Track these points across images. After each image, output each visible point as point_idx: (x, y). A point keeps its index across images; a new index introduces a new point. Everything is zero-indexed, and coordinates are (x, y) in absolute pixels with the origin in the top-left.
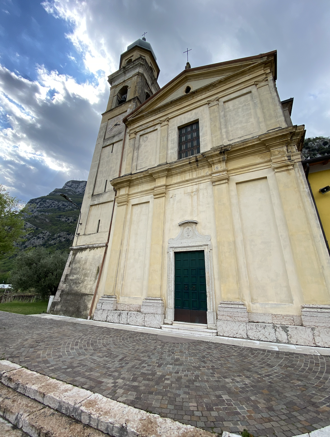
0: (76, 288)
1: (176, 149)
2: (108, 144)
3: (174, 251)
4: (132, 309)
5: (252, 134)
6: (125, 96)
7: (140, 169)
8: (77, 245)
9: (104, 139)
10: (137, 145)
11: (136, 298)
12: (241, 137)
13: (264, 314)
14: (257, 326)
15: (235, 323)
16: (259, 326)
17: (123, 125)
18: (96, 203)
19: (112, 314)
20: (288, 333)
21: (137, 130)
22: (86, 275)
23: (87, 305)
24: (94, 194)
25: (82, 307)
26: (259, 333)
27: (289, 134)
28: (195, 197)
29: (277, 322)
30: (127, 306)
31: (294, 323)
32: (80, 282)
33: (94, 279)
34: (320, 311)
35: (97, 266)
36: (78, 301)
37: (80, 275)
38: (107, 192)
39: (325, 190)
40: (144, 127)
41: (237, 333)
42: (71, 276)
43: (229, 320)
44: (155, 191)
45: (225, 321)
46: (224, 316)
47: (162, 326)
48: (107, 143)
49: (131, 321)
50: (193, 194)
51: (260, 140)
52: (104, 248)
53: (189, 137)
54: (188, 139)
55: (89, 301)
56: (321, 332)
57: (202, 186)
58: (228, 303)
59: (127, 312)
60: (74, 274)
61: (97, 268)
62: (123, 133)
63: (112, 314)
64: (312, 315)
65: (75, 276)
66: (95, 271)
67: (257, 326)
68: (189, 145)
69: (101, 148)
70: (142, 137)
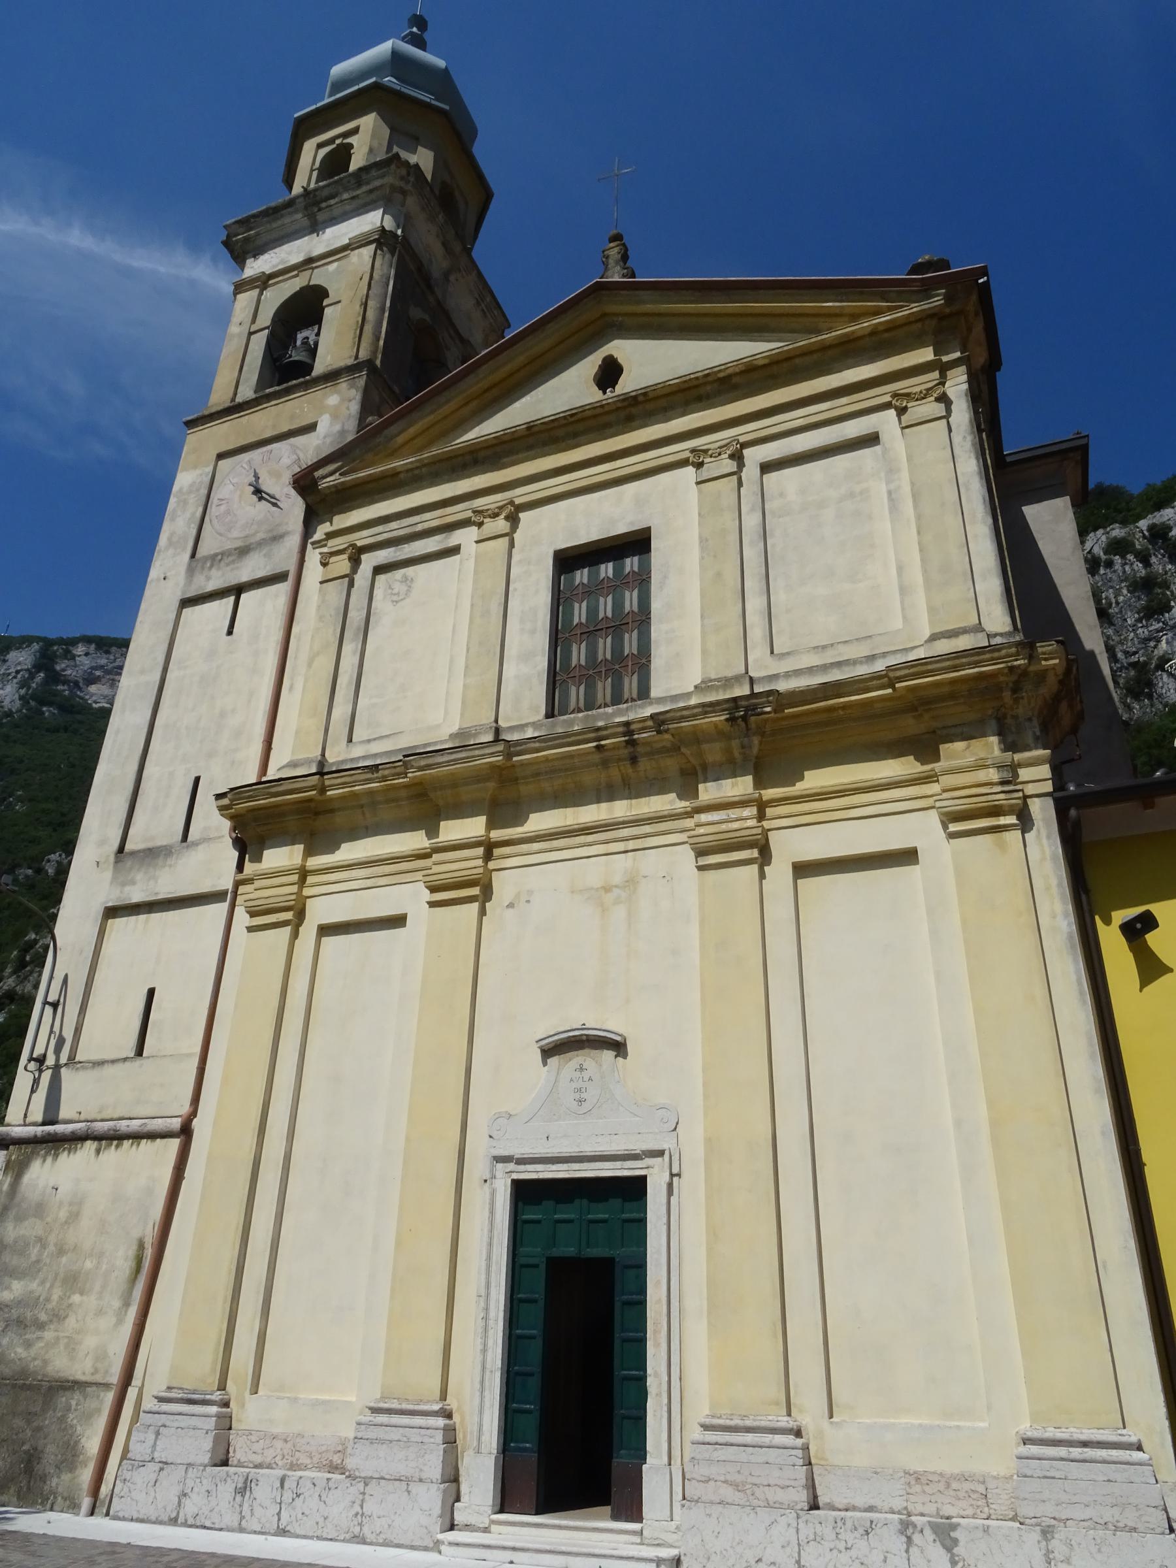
0: (19, 1350)
2: (211, 587)
3: (515, 1176)
4: (303, 1459)
5: (869, 641)
6: (308, 333)
7: (369, 741)
8: (28, 1120)
9: (193, 555)
10: (356, 616)
11: (324, 1402)
12: (824, 647)
13: (876, 1473)
14: (840, 1524)
15: (753, 1515)
16: (849, 1524)
17: (295, 507)
19: (207, 1484)
20: (955, 1550)
21: (362, 538)
22: (73, 1281)
23: (77, 1443)
24: (129, 847)
25: (51, 1452)
27: (1006, 671)
28: (620, 912)
29: (923, 1504)
30: (279, 1444)
31: (986, 1509)
32: (43, 1317)
33: (117, 1304)
34: (1079, 1457)
35: (136, 1234)
36: (29, 1422)
37: (43, 1283)
38: (196, 844)
39: (1139, 926)
41: (759, 1560)
43: (730, 1501)
44: (436, 869)
45: (714, 1507)
46: (712, 1483)
47: (441, 1536)
48: (208, 578)
49: (300, 1516)
50: (609, 898)
52: (175, 1144)
53: (606, 607)
54: (601, 615)
55: (88, 1417)
56: (1076, 1547)
57: (651, 862)
58: (732, 1423)
59: (279, 1473)
61: (135, 1247)
62: (294, 540)
63: (207, 1484)
64: (1048, 1474)
66: (122, 1261)
67: (840, 1524)
68: (605, 648)
69: (176, 604)
70: (381, 579)
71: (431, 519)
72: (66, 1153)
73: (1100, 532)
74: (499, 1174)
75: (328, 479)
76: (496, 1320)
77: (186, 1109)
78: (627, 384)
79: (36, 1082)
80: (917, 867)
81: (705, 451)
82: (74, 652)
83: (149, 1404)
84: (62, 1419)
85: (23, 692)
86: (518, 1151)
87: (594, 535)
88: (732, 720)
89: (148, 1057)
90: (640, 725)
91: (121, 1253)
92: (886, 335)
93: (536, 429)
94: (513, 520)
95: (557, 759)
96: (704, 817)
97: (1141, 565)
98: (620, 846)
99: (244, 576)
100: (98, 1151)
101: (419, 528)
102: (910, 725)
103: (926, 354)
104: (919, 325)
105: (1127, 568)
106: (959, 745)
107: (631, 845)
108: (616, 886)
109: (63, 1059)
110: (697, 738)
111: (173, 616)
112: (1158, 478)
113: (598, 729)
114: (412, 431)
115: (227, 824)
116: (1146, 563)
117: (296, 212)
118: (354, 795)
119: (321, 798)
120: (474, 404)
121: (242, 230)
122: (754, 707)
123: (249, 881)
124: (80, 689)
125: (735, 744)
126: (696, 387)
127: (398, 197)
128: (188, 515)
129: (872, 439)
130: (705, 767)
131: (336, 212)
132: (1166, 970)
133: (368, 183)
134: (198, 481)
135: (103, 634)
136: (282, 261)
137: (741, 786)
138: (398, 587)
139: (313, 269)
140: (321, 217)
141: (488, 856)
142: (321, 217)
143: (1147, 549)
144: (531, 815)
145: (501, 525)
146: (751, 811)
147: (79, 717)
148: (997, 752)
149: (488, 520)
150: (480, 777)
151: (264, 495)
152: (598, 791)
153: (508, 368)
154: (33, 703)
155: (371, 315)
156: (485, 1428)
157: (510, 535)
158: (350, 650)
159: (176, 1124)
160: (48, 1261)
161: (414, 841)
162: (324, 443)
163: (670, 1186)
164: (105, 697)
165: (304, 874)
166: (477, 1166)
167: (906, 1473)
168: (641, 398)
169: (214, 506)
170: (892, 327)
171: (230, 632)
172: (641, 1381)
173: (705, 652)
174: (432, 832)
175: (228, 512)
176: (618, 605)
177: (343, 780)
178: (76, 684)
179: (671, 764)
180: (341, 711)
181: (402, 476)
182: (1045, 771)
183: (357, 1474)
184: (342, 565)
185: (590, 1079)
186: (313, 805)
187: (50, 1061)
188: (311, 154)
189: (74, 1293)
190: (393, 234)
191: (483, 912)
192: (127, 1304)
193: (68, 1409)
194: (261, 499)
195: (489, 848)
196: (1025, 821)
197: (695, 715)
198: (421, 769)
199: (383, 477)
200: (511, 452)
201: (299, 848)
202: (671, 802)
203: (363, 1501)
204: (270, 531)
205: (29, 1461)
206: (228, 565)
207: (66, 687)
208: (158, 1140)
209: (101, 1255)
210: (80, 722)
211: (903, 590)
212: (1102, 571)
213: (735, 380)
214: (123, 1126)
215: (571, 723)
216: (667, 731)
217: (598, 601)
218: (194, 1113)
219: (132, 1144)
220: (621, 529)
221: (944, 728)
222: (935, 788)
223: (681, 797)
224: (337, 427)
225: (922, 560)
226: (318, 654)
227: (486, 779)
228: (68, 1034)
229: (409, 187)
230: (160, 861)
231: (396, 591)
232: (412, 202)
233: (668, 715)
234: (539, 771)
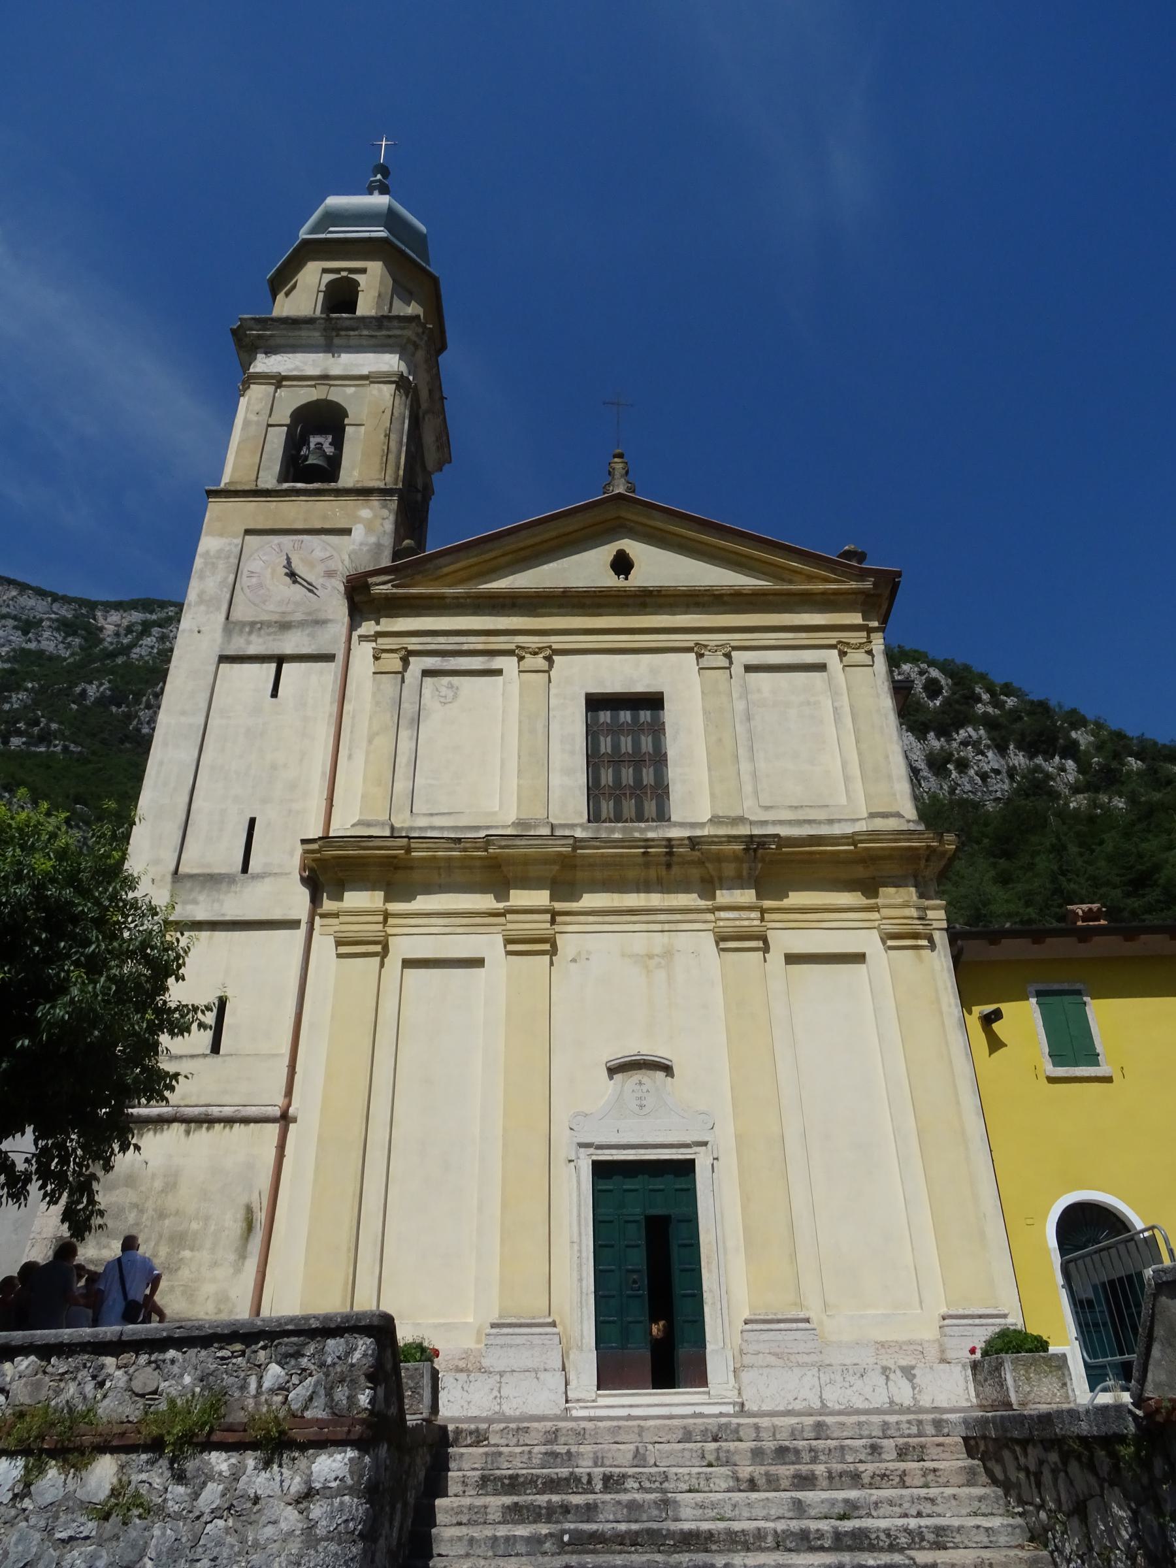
1: (581, 779)
2: (252, 650)
3: (595, 1158)
9: (227, 618)
10: (408, 707)
12: (796, 807)
14: (845, 1372)
15: (790, 1372)
20: (915, 1381)
21: (413, 643)
26: (849, 1392)
33: (232, 1257)
35: (243, 1200)
38: (256, 877)
41: (796, 1399)
44: (510, 926)
48: (249, 643)
50: (652, 963)
51: (855, 844)
52: (273, 1129)
57: (682, 941)
66: (233, 1224)
67: (845, 1372)
70: (428, 681)
72: (151, 1133)
74: (582, 1156)
75: (381, 587)
76: (588, 1259)
77: (280, 1100)
78: (639, 578)
80: (482, 969)
81: (706, 646)
87: (618, 688)
88: (746, 850)
89: (222, 1056)
90: (678, 842)
92: (832, 597)
93: (569, 594)
95: (612, 856)
96: (723, 914)
98: (658, 927)
99: (288, 650)
100: (188, 1133)
101: (465, 647)
102: (860, 872)
103: (856, 618)
104: (854, 596)
106: (892, 890)
107: (667, 927)
108: (657, 955)
110: (719, 858)
111: (213, 668)
113: (647, 840)
118: (434, 857)
119: (406, 857)
120: (509, 558)
121: (259, 327)
122: (764, 843)
125: (745, 866)
126: (698, 595)
127: (411, 348)
128: (219, 578)
129: (821, 667)
130: (720, 879)
131: (353, 342)
132: (1004, 1045)
133: (388, 329)
134: (228, 549)
137: (747, 896)
138: (444, 691)
139: (331, 385)
140: (337, 341)
142: (337, 341)
144: (584, 895)
146: (755, 914)
148: (915, 898)
149: (528, 655)
150: (547, 860)
151: (299, 580)
156: (585, 1333)
158: (404, 734)
159: (277, 1112)
160: (149, 1223)
161: (485, 902)
162: (360, 549)
167: (876, 1342)
168: (655, 593)
169: (244, 577)
170: (836, 593)
171: (275, 693)
173: (713, 795)
176: (636, 744)
177: (424, 845)
179: (695, 873)
181: (448, 601)
182: (941, 914)
183: (492, 1369)
184: (393, 662)
185: (648, 1091)
186: (395, 861)
189: (184, 1249)
191: (382, 965)
192: (242, 1255)
194: (295, 582)
196: (932, 946)
197: (721, 842)
198: (501, 847)
199: (431, 597)
200: (544, 606)
201: (379, 895)
202: (694, 900)
203: (500, 1387)
204: (309, 614)
206: (269, 634)
208: (252, 1125)
209: (207, 1219)
211: (847, 779)
213: (725, 598)
214: (215, 1111)
215: (613, 830)
216: (699, 850)
217: (619, 739)
219: (224, 1127)
220: (640, 688)
221: (882, 877)
222: (876, 915)
223: (701, 897)
224: (372, 539)
225: (860, 761)
226: (377, 734)
227: (554, 862)
229: (422, 343)
230: (224, 886)
231: (443, 694)
233: (703, 839)
234: (592, 864)
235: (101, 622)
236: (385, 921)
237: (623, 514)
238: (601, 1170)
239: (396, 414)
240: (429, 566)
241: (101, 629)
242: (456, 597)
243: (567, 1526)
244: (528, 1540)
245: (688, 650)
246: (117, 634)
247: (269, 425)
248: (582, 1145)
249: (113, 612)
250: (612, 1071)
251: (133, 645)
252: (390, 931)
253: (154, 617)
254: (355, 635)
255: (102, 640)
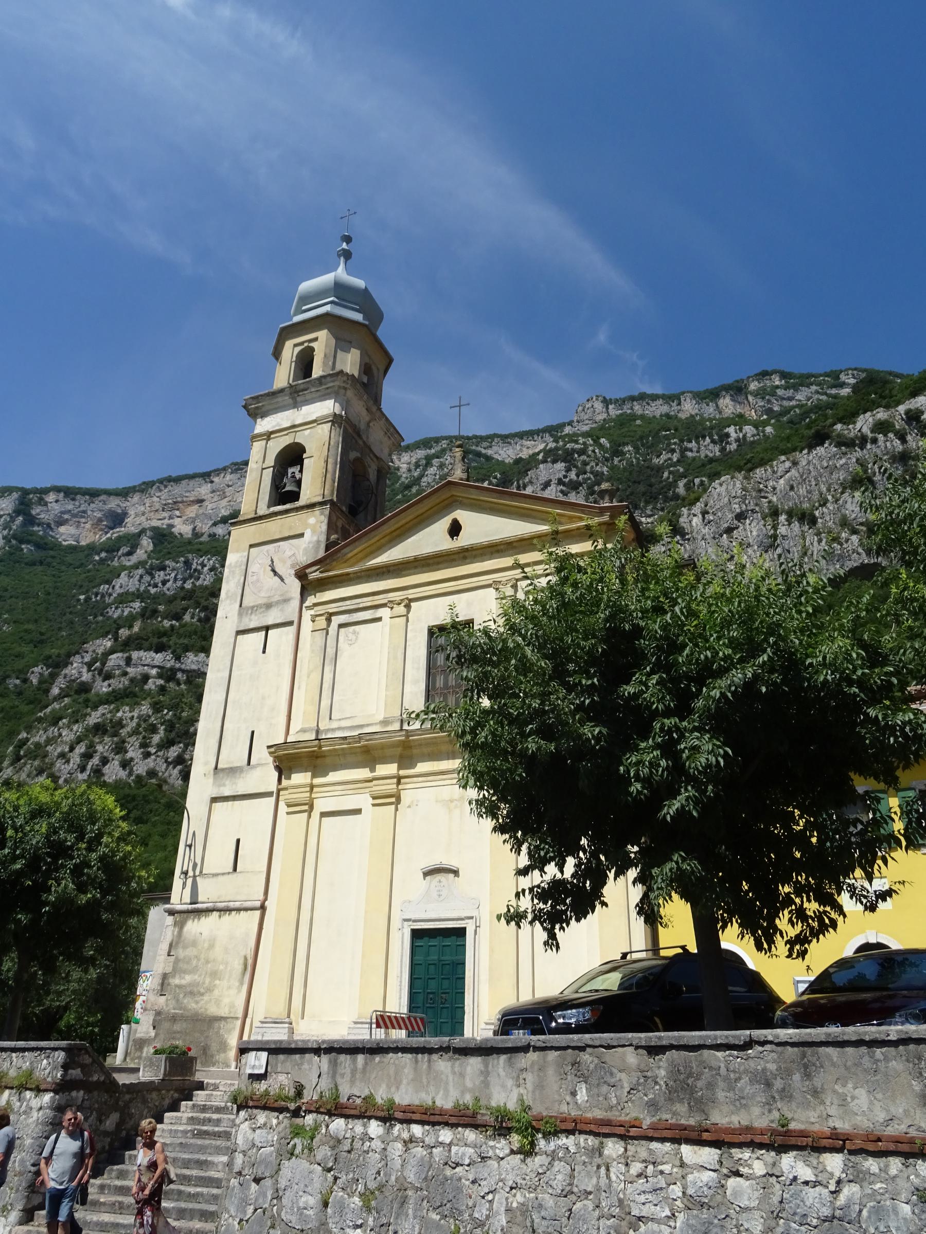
2: (252, 626)
9: (241, 606)
10: (330, 651)
17: (296, 585)
18: (227, 792)
21: (332, 608)
22: (215, 975)
24: (220, 766)
25: (214, 1047)
32: (202, 990)
33: (237, 984)
35: (243, 953)
37: (200, 976)
38: (255, 767)
40: (348, 605)
42: (177, 976)
44: (375, 788)
48: (250, 620)
52: (257, 913)
55: (230, 1031)
60: (185, 972)
65: (188, 979)
66: (238, 966)
70: (342, 630)
71: (367, 602)
73: (869, 414)
77: (262, 897)
78: (465, 539)
79: (184, 884)
81: (500, 582)
82: (47, 500)
83: (256, 1023)
84: (218, 1033)
85: (5, 532)
86: (413, 917)
91: (236, 962)
94: (408, 607)
97: (899, 442)
99: (270, 623)
100: (220, 917)
101: (361, 606)
105: (888, 444)
109: (197, 873)
111: (233, 640)
112: (913, 369)
114: (355, 551)
115: (271, 759)
116: (903, 440)
117: (285, 395)
120: (387, 539)
123: (285, 789)
124: (52, 529)
127: (342, 391)
128: (236, 580)
131: (308, 397)
135: (70, 485)
136: (278, 424)
138: (350, 635)
139: (296, 432)
140: (299, 399)
141: (399, 783)
142: (299, 399)
143: (904, 429)
145: (401, 609)
147: (52, 553)
152: (448, 753)
153: (404, 522)
154: (14, 542)
155: (330, 467)
157: (407, 616)
158: (328, 669)
159: (258, 904)
161: (363, 773)
163: (476, 931)
164: (72, 536)
165: (312, 787)
166: (396, 923)
171: (264, 652)
172: (463, 1008)
174: (373, 770)
175: (258, 581)
178: (49, 525)
180: (325, 703)
184: (322, 623)
187: (191, 873)
188: (290, 351)
190: (341, 416)
191: (397, 809)
192: (242, 984)
193: (219, 1028)
195: (399, 779)
198: (367, 740)
199: (342, 575)
201: (309, 774)
204: (281, 595)
205: (204, 1050)
207: (40, 528)
210: (53, 557)
212: (869, 446)
214: (232, 905)
218: (266, 899)
224: (315, 538)
227: (398, 746)
228: (199, 861)
230: (237, 775)
232: (350, 393)
235: (397, 463)
236: (311, 791)
237: (455, 493)
238: (417, 934)
239: (332, 443)
240: (339, 555)
241: (398, 469)
242: (355, 573)
243: (197, 1127)
244: (182, 1132)
245: (489, 586)
246: (409, 470)
247: (263, 469)
248: (405, 920)
249: (404, 454)
250: (428, 873)
251: (422, 476)
252: (314, 796)
253: (433, 451)
254: (305, 605)
255: (399, 477)
